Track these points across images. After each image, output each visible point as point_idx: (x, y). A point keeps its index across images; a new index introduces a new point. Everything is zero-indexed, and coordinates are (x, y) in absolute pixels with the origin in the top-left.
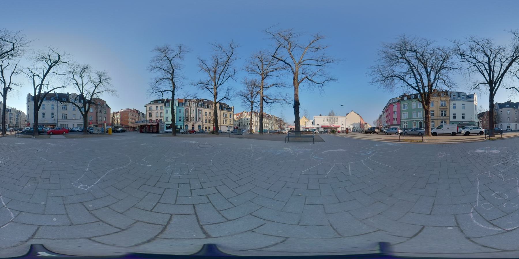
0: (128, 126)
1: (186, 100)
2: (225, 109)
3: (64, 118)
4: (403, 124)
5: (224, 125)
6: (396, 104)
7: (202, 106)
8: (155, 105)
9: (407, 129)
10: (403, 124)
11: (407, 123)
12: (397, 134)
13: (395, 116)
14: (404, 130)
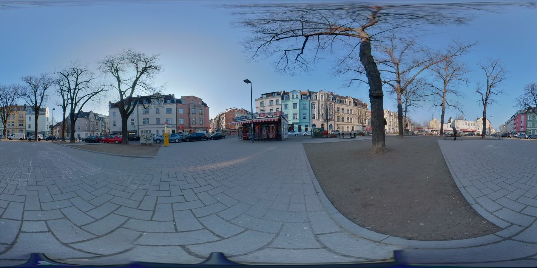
0: (236, 130)
1: (310, 93)
2: (360, 106)
3: (169, 112)
4: (528, 132)
5: (359, 124)
6: (523, 115)
7: (333, 100)
8: (268, 99)
9: (531, 135)
10: (528, 132)
11: (531, 131)
12: (525, 138)
13: (522, 124)
14: (529, 136)
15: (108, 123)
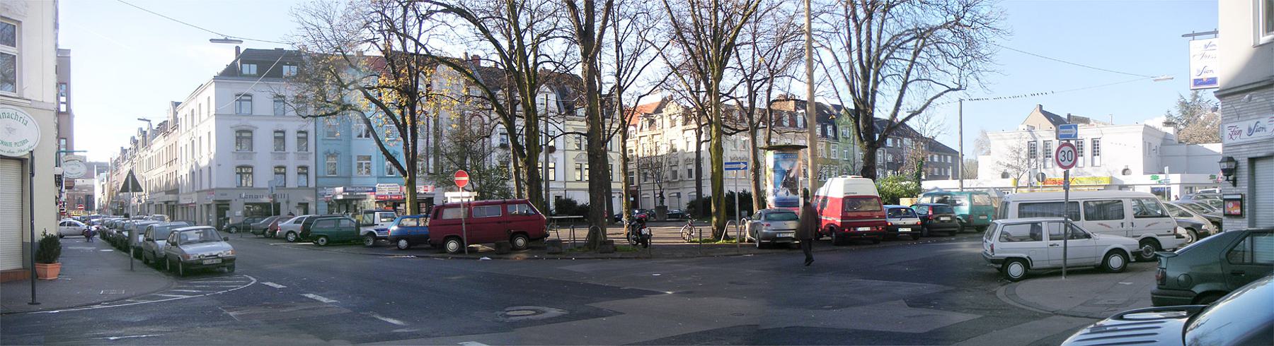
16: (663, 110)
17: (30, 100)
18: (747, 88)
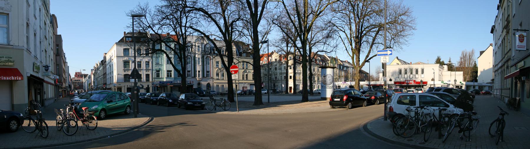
5: (243, 81)
15: (119, 85)
16: (272, 55)
17: (13, 46)
18: (251, 67)
